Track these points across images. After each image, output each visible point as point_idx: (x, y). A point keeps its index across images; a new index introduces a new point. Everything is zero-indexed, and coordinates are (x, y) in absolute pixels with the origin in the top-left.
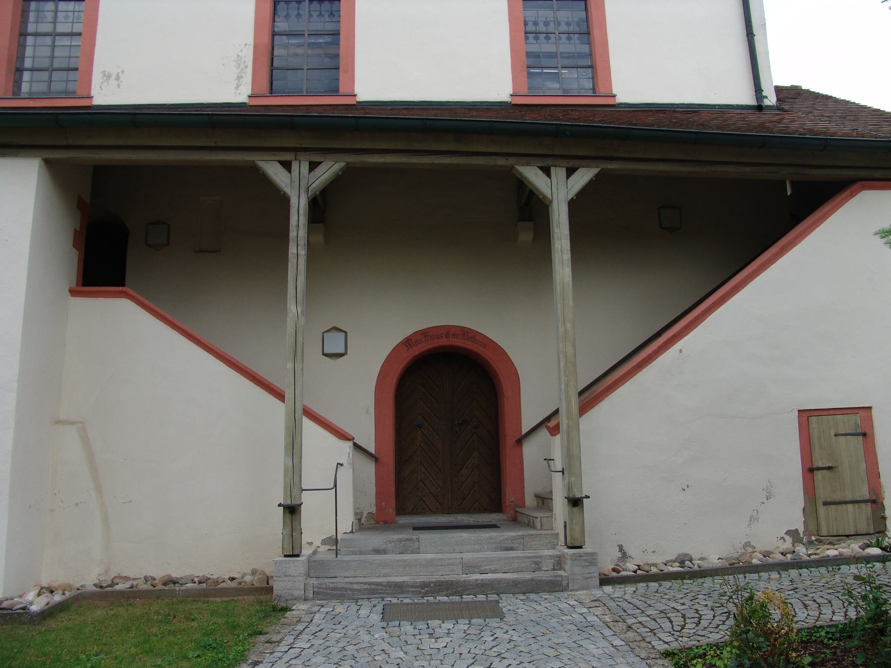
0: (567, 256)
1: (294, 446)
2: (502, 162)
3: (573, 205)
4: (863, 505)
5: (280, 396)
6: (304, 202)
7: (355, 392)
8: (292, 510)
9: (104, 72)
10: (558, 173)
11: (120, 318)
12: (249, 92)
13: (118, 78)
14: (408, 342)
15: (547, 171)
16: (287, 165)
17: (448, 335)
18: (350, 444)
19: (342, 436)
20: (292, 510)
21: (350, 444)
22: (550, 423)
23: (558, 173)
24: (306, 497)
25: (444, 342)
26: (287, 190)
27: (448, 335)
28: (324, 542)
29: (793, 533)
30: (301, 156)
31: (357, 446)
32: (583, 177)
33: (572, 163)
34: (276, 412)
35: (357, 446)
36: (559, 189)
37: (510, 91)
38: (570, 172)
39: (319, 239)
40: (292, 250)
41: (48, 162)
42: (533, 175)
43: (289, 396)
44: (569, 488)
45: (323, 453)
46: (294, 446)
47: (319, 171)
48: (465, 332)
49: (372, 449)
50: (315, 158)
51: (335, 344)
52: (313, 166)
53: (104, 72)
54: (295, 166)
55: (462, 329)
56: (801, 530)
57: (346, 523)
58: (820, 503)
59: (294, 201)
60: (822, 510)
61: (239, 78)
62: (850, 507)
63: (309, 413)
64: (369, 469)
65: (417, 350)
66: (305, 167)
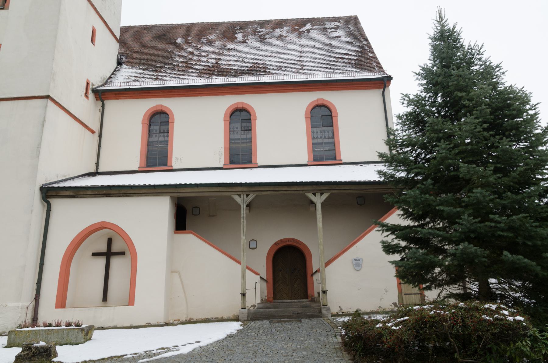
0: (321, 220)
1: (244, 276)
2: (301, 192)
3: (322, 204)
4: (418, 295)
5: (240, 263)
6: (245, 206)
7: (261, 261)
8: (244, 295)
9: (176, 158)
10: (318, 195)
11: (189, 239)
12: (223, 163)
13: (181, 160)
14: (276, 244)
15: (314, 194)
16: (239, 195)
17: (289, 241)
18: (258, 276)
19: (257, 274)
20: (244, 295)
21: (258, 276)
22: (318, 271)
23: (318, 195)
24: (247, 291)
25: (288, 243)
26: (240, 203)
27: (289, 241)
28: (252, 306)
29: (395, 304)
30: (244, 193)
31: (261, 278)
32: (325, 196)
33: (322, 191)
34: (238, 268)
35: (261, 278)
36: (319, 200)
37: (307, 160)
38: (322, 194)
39: (248, 211)
40: (242, 220)
41: (171, 197)
42: (311, 196)
43: (242, 262)
44: (322, 288)
45: (252, 279)
46: (244, 276)
47: (249, 197)
48: (294, 240)
49: (265, 278)
50: (248, 193)
51: (253, 245)
52: (247, 196)
53: (176, 158)
54: (242, 196)
55: (293, 239)
56: (397, 303)
57: (258, 301)
58: (403, 294)
59: (242, 206)
60: (404, 296)
61: (220, 159)
62: (413, 296)
63: (248, 268)
64: (265, 284)
65: (279, 246)
66: (245, 196)
